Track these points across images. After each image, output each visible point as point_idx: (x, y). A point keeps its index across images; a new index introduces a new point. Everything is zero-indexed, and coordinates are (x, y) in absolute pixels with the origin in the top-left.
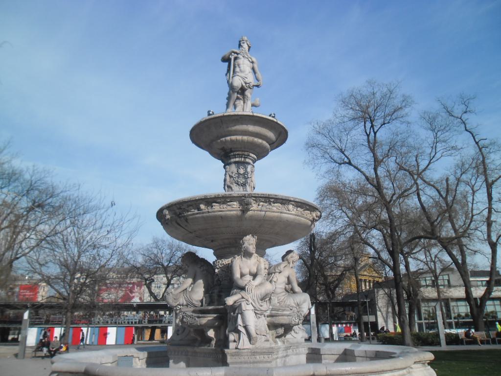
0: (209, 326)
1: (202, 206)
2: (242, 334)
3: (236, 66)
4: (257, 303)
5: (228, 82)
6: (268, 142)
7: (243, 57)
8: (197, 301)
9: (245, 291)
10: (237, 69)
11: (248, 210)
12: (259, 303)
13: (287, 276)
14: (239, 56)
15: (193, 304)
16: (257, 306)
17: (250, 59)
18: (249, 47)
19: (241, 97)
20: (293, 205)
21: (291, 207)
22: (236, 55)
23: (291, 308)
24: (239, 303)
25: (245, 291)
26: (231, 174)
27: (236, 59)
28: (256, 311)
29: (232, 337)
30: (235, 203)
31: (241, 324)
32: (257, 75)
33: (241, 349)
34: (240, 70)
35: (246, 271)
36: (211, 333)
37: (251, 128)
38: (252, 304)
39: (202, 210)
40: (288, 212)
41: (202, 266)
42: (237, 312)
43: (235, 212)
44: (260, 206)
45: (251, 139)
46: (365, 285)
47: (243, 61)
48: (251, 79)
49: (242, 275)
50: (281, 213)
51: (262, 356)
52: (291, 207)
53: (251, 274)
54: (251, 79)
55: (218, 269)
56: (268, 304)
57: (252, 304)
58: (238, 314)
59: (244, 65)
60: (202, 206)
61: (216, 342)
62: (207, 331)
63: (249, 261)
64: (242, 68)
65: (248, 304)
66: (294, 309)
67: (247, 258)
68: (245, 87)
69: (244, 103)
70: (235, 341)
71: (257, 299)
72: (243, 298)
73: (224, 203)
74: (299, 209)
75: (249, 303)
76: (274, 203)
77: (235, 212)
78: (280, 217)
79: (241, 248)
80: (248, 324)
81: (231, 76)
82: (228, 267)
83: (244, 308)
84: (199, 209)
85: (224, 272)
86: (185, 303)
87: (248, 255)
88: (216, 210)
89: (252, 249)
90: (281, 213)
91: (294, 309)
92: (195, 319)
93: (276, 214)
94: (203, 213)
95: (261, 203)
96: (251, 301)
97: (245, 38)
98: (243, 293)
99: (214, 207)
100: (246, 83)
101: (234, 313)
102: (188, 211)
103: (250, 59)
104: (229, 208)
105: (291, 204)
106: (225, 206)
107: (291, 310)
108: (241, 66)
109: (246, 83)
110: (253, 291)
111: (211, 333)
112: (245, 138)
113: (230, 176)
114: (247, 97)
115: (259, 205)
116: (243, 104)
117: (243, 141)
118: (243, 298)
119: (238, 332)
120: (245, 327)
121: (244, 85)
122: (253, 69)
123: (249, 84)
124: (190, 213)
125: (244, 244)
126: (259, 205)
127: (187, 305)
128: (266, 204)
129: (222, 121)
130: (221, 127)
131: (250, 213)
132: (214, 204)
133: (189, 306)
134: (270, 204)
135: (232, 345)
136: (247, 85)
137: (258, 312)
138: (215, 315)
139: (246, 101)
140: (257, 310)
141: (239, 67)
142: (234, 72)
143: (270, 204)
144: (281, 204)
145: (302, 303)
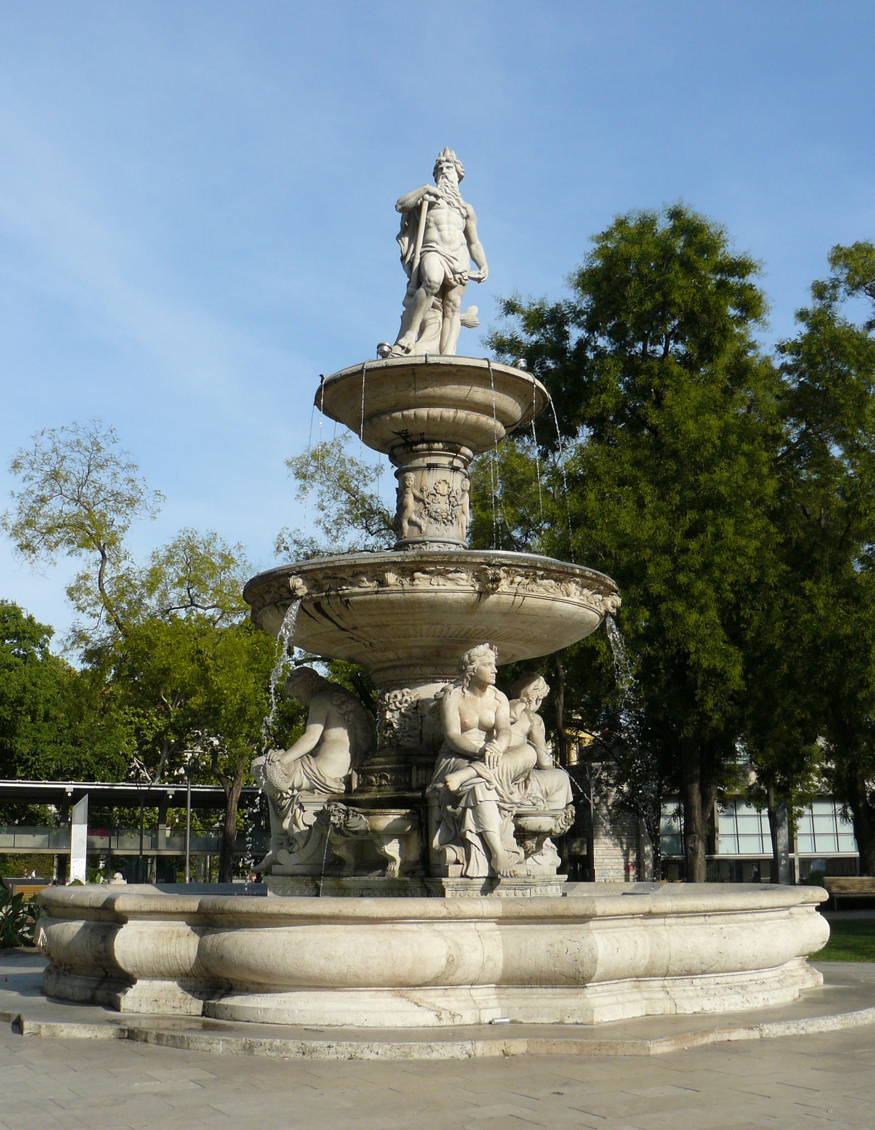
0: (390, 834)
1: (391, 578)
2: (473, 848)
3: (431, 224)
4: (506, 788)
5: (403, 258)
6: (503, 423)
7: (448, 203)
8: (335, 780)
9: (484, 762)
10: (434, 234)
11: (493, 591)
12: (508, 786)
13: (527, 730)
14: (440, 201)
15: (326, 787)
16: (505, 793)
17: (463, 211)
18: (461, 178)
19: (439, 304)
20: (577, 583)
21: (573, 587)
22: (433, 199)
23: (535, 801)
24: (470, 787)
25: (484, 762)
26: (418, 494)
27: (431, 206)
28: (502, 804)
29: (452, 853)
30: (464, 576)
31: (473, 829)
32: (473, 247)
33: (471, 878)
34: (442, 237)
35: (473, 719)
36: (392, 849)
37: (479, 394)
38: (496, 789)
39: (388, 586)
40: (566, 598)
41: (343, 703)
42: (462, 804)
43: (462, 595)
44: (515, 585)
45: (474, 417)
46: (381, 763)
47: (448, 214)
48: (463, 264)
49: (465, 728)
50: (554, 600)
51: (512, 892)
52: (573, 587)
53: (482, 726)
54: (463, 264)
55: (391, 711)
56: (523, 791)
57: (496, 789)
58: (464, 809)
59: (447, 223)
60: (391, 578)
61: (401, 865)
62: (383, 844)
63: (479, 699)
64: (445, 233)
65: (489, 789)
66: (539, 804)
67: (475, 694)
68: (452, 281)
69: (444, 317)
70: (457, 862)
71: (508, 780)
72: (479, 776)
73: (442, 574)
74: (586, 591)
75: (492, 787)
76: (542, 578)
77: (462, 595)
78: (550, 609)
79: (465, 671)
80: (487, 828)
81: (419, 249)
82: (416, 708)
83: (480, 797)
84: (382, 583)
85: (407, 720)
86: (306, 784)
87: (477, 685)
88: (420, 587)
89: (490, 673)
90: (554, 600)
91: (539, 804)
92: (361, 818)
93: (541, 602)
94: (391, 592)
95: (518, 579)
96: (496, 783)
97: (451, 154)
98: (479, 766)
99: (417, 582)
100: (454, 272)
101: (455, 807)
102: (352, 584)
103: (463, 211)
104: (450, 585)
105: (575, 582)
106: (441, 581)
107: (534, 805)
108: (444, 227)
109: (454, 272)
110: (500, 763)
111: (392, 849)
112: (462, 414)
113: (416, 498)
114: (454, 305)
115: (512, 582)
116: (441, 319)
117: (455, 422)
118: (479, 776)
119: (466, 845)
120: (482, 836)
121: (450, 276)
122: (466, 232)
123: (461, 273)
124: (357, 589)
125: (472, 662)
126: (512, 582)
127: (311, 790)
128: (527, 581)
129: (414, 374)
130: (410, 386)
131: (493, 598)
132: (418, 574)
133: (316, 791)
134: (534, 580)
135: (454, 870)
136: (457, 276)
137: (507, 806)
138: (403, 811)
139: (450, 314)
140: (504, 802)
141: (439, 230)
142: (426, 241)
143: (534, 580)
144: (556, 581)
145: (554, 790)
